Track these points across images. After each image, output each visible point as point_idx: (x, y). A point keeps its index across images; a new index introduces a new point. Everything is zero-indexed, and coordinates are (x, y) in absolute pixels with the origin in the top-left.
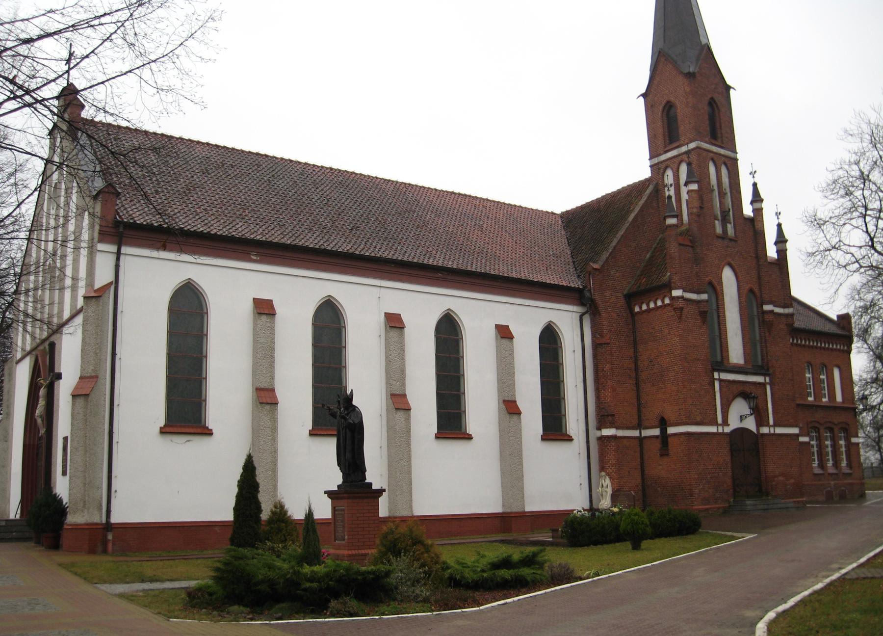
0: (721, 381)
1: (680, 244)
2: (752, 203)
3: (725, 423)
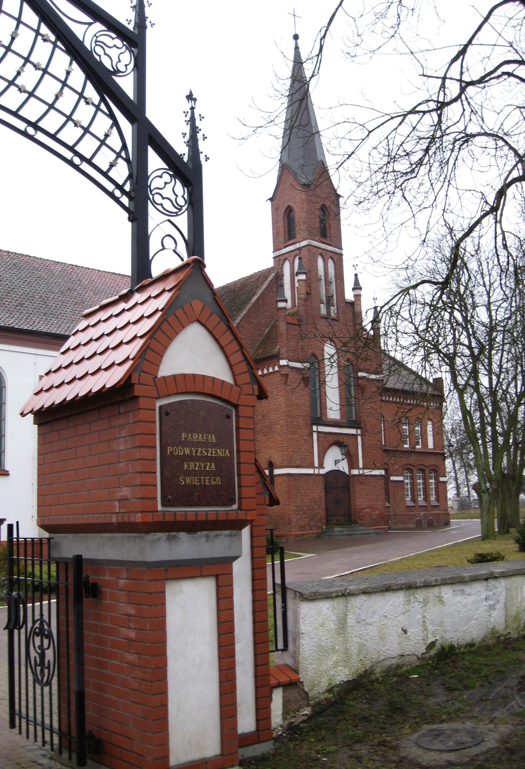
0: (318, 432)
1: (288, 323)
2: (354, 289)
3: (321, 466)
